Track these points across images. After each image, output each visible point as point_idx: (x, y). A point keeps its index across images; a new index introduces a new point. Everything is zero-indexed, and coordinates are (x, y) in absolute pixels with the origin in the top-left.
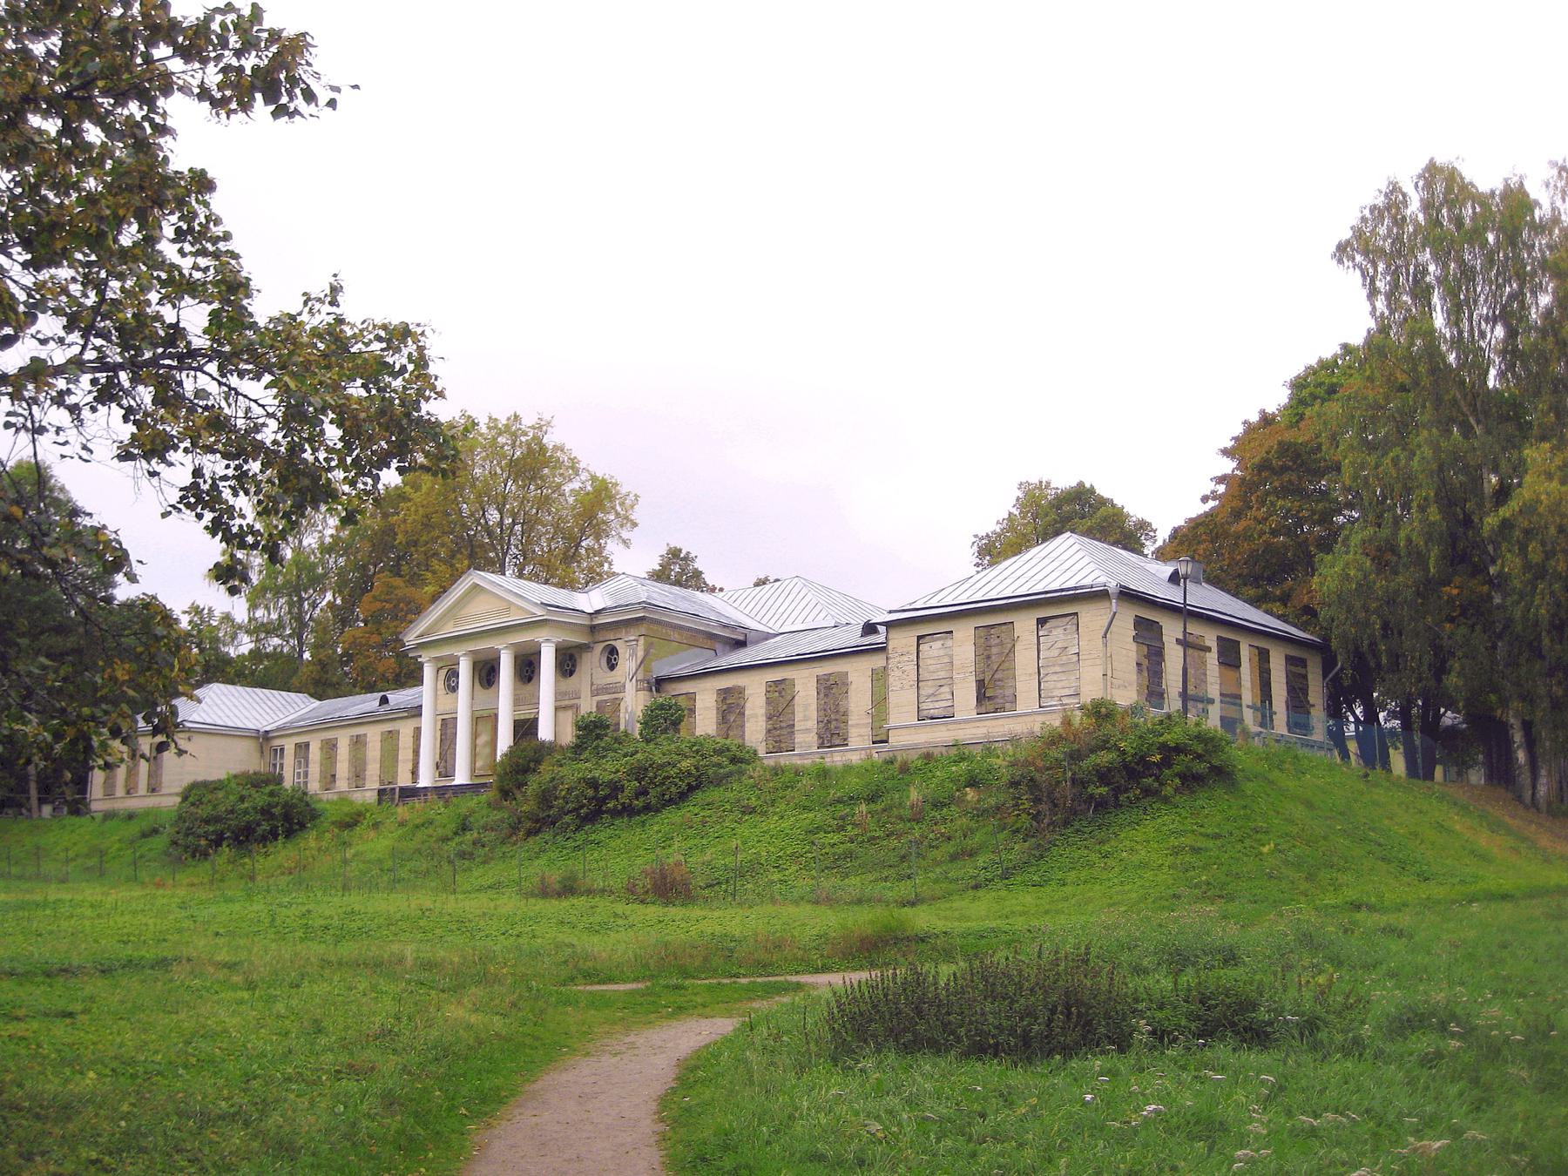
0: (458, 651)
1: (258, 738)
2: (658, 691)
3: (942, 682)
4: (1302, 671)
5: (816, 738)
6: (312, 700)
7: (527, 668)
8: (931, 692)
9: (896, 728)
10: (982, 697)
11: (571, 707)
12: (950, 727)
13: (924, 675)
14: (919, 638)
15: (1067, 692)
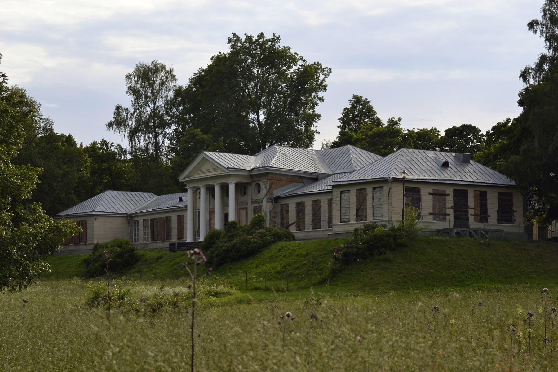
0: (199, 185)
1: (127, 217)
3: (348, 209)
6: (154, 195)
8: (344, 212)
9: (334, 225)
10: (357, 215)
11: (245, 208)
12: (349, 225)
13: (343, 206)
14: (341, 192)
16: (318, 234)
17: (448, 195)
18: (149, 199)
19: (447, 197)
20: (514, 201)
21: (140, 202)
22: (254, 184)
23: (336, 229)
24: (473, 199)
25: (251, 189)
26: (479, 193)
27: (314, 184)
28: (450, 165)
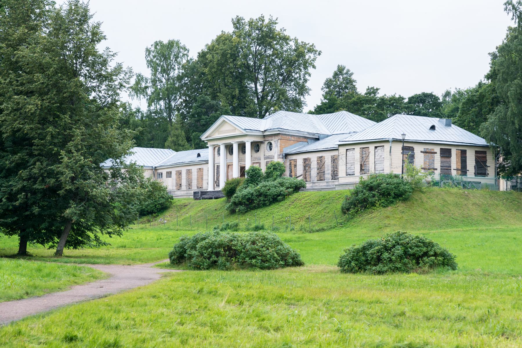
1: (152, 169)
2: (285, 158)
3: (352, 164)
4: (484, 155)
5: (331, 176)
6: (174, 152)
7: (242, 147)
8: (349, 167)
10: (361, 170)
14: (347, 150)
15: (381, 169)
16: (322, 184)
17: (436, 153)
18: (169, 154)
19: (435, 154)
20: (487, 159)
21: (162, 157)
22: (267, 142)
23: (342, 181)
24: (455, 156)
25: (264, 147)
26: (460, 151)
27: (318, 143)
28: (436, 128)
